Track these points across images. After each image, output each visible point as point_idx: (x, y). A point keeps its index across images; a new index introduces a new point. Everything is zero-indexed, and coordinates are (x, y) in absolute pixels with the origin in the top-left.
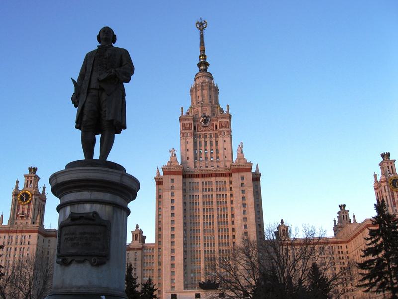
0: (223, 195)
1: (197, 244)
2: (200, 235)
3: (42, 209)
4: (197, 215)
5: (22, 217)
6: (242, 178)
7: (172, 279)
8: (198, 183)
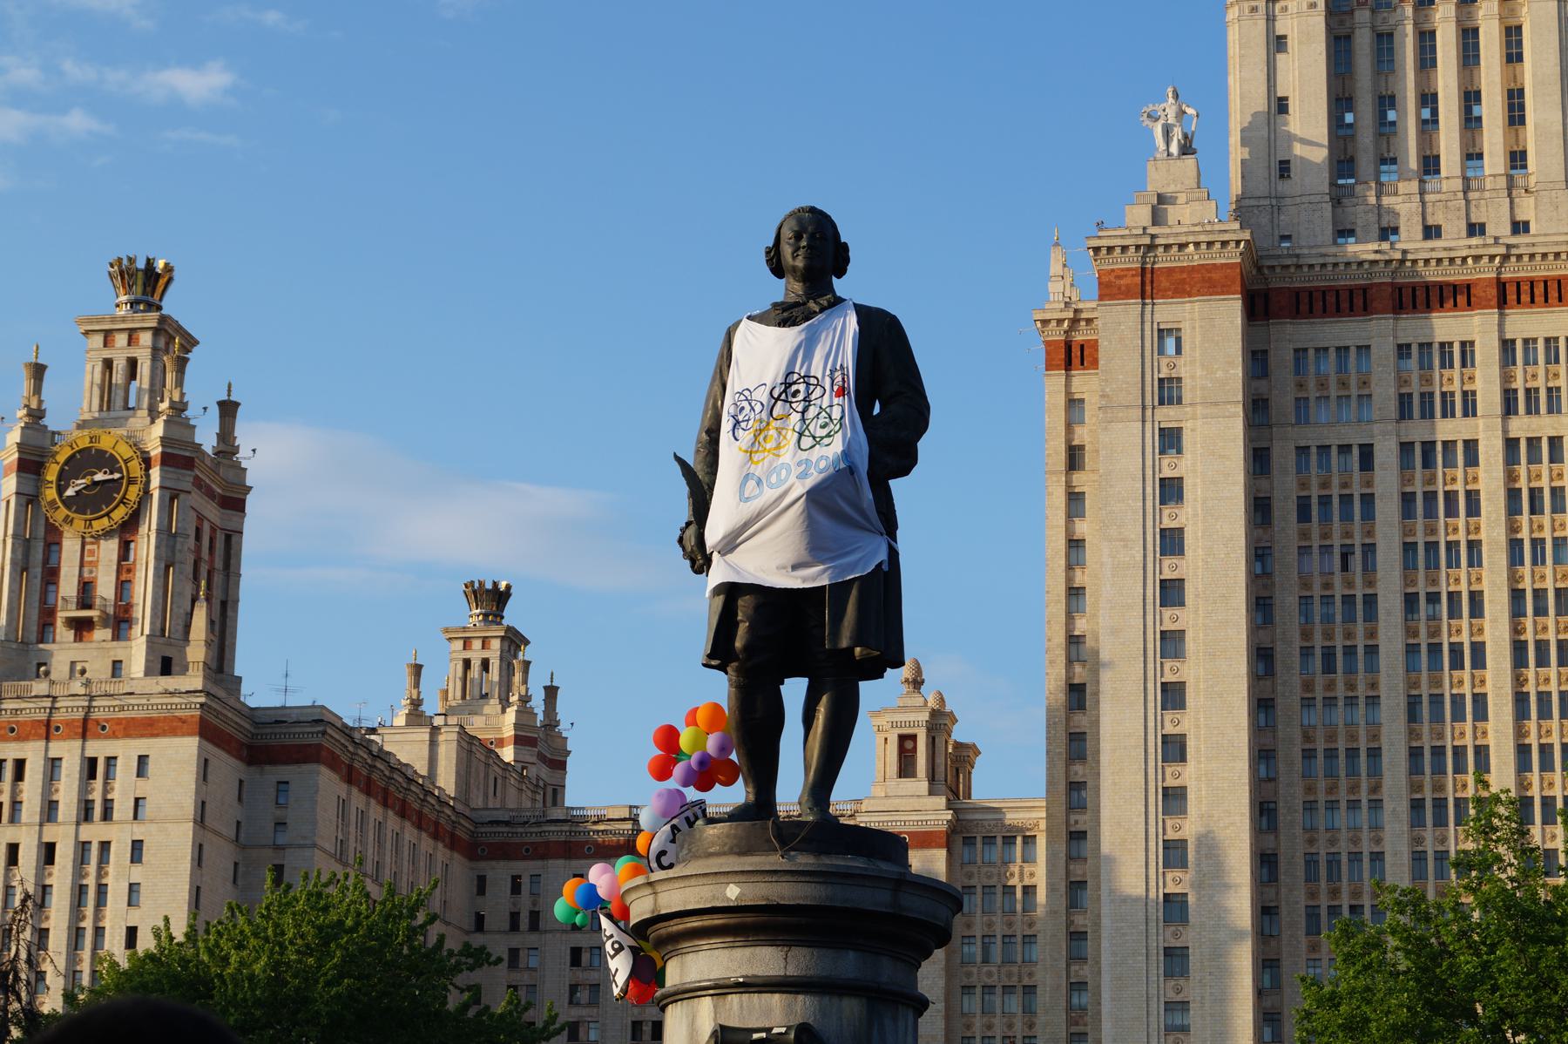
1: (1354, 805)
2: (1372, 634)
3: (219, 564)
5: (81, 627)
7: (1170, 1006)
8: (1364, 349)
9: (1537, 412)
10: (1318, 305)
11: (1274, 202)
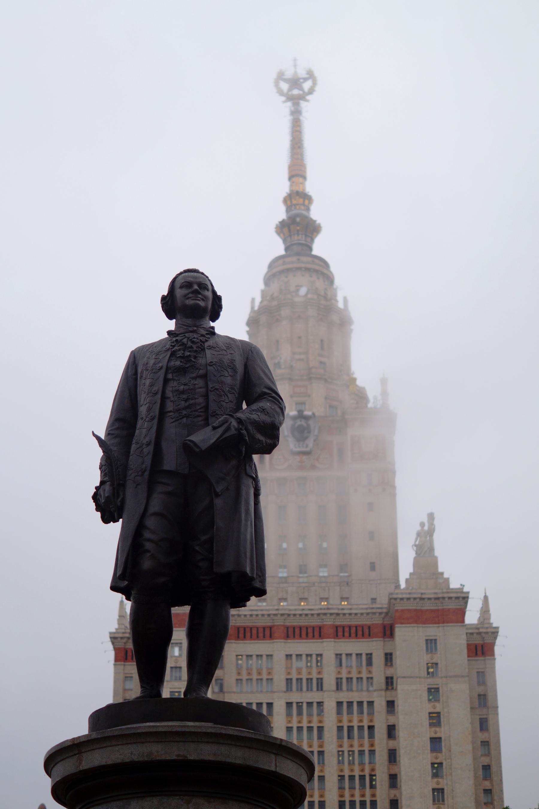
6: (431, 644)
9: (312, 690)
10: (248, 634)
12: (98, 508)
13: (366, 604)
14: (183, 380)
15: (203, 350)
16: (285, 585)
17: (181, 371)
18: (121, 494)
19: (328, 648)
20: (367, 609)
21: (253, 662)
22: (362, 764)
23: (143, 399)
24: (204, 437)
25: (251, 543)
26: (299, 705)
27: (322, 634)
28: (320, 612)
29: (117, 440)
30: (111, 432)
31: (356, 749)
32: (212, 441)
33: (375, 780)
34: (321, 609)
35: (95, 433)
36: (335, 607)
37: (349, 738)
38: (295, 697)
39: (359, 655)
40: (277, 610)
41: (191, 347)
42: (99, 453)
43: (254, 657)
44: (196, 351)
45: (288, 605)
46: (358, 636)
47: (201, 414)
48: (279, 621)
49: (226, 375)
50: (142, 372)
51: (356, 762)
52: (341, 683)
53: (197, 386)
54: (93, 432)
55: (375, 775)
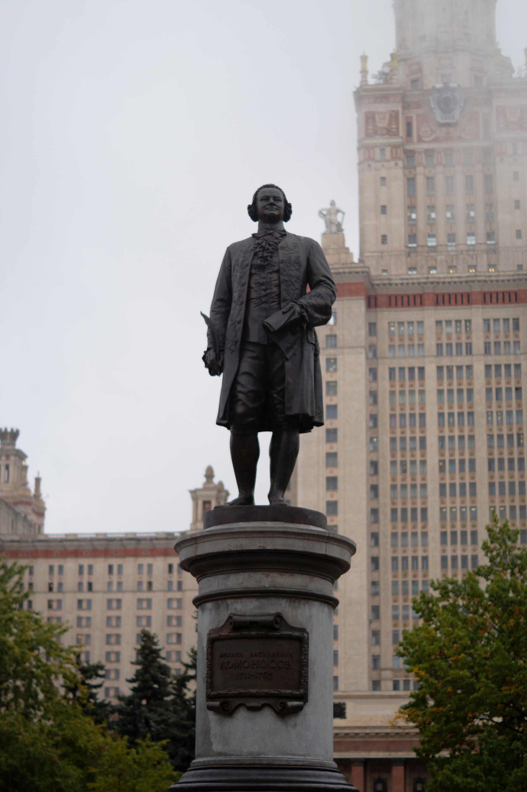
0: (508, 366)
4: (418, 435)
9: (461, 354)
10: (399, 302)
11: (379, 254)
12: (207, 366)
13: (513, 271)
14: (263, 275)
15: (277, 250)
16: (434, 254)
17: (262, 268)
18: (222, 357)
19: (477, 314)
20: (513, 275)
21: (405, 329)
22: (510, 424)
23: (236, 287)
24: (276, 320)
25: (312, 392)
26: (450, 369)
27: (470, 300)
28: (468, 279)
29: (219, 316)
30: (214, 310)
31: (504, 409)
32: (282, 323)
33: (523, 439)
34: (469, 276)
35: (203, 313)
36: (482, 274)
37: (497, 398)
38: (445, 361)
39: (506, 320)
40: (427, 278)
41: (268, 249)
42: (205, 328)
43: (406, 325)
44: (272, 252)
45: (437, 273)
46: (505, 301)
47: (276, 300)
48: (429, 289)
49: (293, 269)
50: (234, 267)
51: (505, 421)
52: (490, 347)
53: (272, 279)
54: (201, 313)
55: (523, 434)
